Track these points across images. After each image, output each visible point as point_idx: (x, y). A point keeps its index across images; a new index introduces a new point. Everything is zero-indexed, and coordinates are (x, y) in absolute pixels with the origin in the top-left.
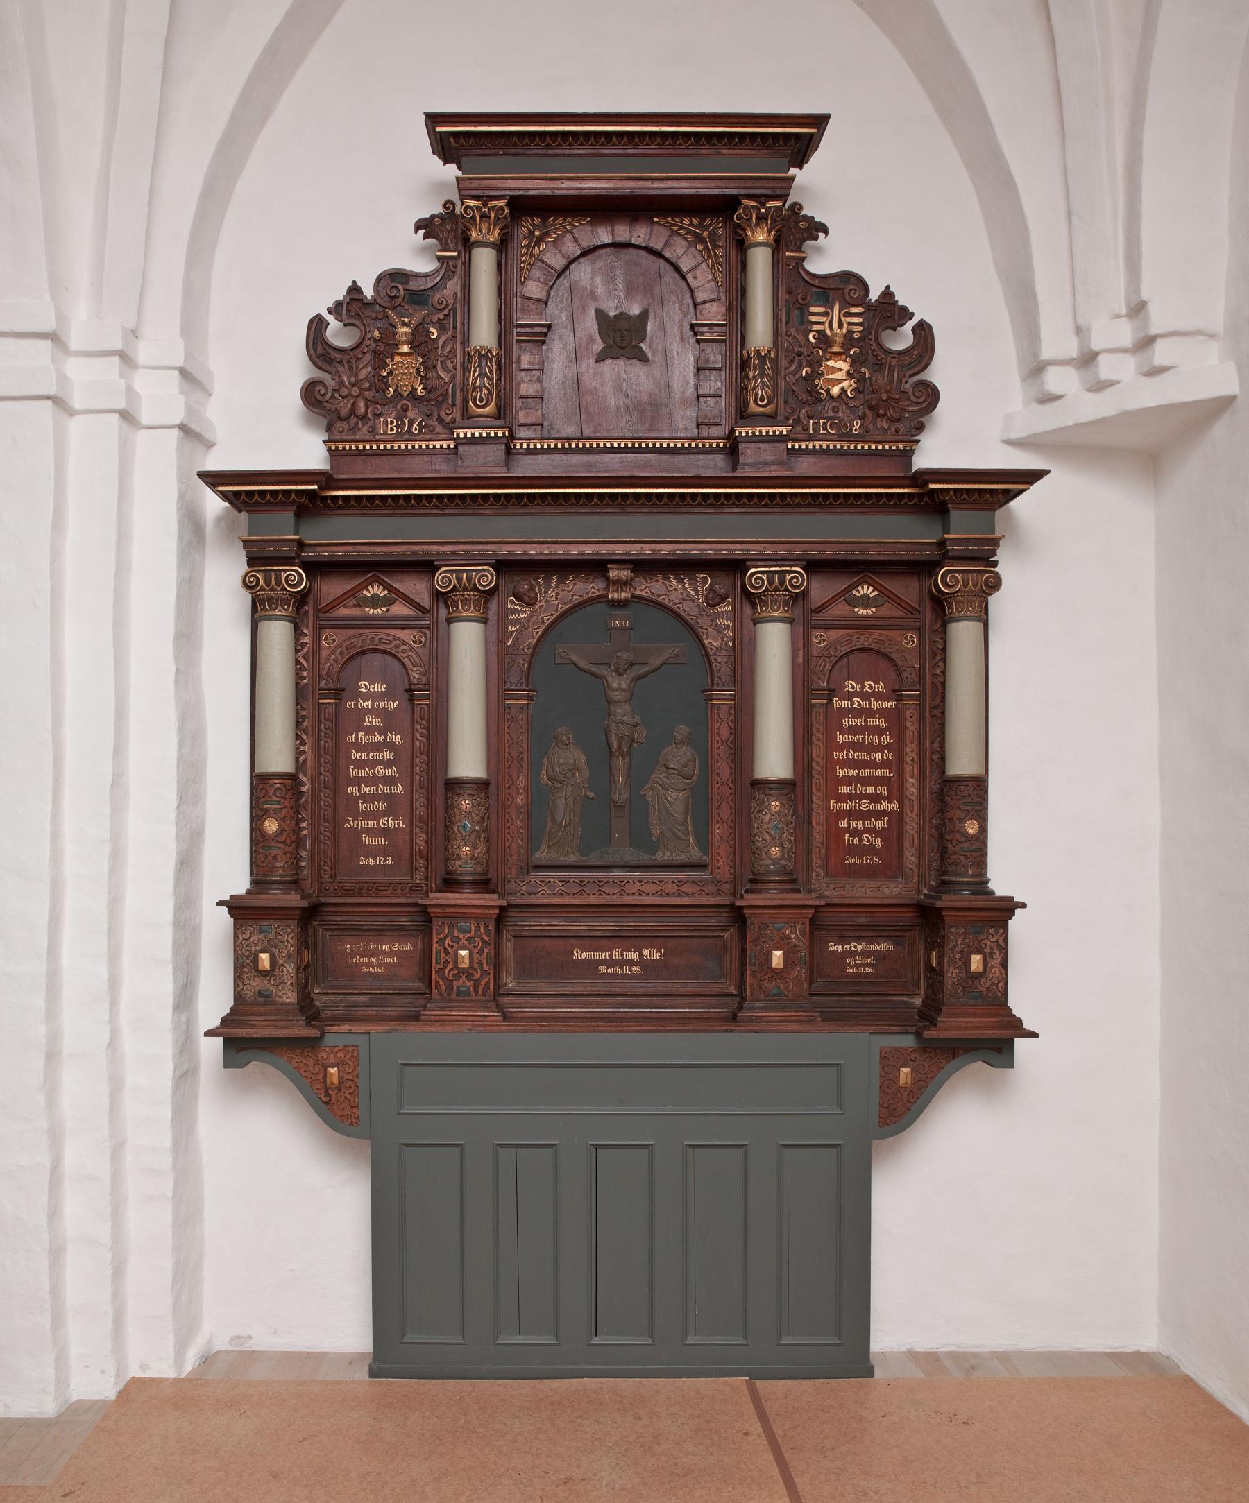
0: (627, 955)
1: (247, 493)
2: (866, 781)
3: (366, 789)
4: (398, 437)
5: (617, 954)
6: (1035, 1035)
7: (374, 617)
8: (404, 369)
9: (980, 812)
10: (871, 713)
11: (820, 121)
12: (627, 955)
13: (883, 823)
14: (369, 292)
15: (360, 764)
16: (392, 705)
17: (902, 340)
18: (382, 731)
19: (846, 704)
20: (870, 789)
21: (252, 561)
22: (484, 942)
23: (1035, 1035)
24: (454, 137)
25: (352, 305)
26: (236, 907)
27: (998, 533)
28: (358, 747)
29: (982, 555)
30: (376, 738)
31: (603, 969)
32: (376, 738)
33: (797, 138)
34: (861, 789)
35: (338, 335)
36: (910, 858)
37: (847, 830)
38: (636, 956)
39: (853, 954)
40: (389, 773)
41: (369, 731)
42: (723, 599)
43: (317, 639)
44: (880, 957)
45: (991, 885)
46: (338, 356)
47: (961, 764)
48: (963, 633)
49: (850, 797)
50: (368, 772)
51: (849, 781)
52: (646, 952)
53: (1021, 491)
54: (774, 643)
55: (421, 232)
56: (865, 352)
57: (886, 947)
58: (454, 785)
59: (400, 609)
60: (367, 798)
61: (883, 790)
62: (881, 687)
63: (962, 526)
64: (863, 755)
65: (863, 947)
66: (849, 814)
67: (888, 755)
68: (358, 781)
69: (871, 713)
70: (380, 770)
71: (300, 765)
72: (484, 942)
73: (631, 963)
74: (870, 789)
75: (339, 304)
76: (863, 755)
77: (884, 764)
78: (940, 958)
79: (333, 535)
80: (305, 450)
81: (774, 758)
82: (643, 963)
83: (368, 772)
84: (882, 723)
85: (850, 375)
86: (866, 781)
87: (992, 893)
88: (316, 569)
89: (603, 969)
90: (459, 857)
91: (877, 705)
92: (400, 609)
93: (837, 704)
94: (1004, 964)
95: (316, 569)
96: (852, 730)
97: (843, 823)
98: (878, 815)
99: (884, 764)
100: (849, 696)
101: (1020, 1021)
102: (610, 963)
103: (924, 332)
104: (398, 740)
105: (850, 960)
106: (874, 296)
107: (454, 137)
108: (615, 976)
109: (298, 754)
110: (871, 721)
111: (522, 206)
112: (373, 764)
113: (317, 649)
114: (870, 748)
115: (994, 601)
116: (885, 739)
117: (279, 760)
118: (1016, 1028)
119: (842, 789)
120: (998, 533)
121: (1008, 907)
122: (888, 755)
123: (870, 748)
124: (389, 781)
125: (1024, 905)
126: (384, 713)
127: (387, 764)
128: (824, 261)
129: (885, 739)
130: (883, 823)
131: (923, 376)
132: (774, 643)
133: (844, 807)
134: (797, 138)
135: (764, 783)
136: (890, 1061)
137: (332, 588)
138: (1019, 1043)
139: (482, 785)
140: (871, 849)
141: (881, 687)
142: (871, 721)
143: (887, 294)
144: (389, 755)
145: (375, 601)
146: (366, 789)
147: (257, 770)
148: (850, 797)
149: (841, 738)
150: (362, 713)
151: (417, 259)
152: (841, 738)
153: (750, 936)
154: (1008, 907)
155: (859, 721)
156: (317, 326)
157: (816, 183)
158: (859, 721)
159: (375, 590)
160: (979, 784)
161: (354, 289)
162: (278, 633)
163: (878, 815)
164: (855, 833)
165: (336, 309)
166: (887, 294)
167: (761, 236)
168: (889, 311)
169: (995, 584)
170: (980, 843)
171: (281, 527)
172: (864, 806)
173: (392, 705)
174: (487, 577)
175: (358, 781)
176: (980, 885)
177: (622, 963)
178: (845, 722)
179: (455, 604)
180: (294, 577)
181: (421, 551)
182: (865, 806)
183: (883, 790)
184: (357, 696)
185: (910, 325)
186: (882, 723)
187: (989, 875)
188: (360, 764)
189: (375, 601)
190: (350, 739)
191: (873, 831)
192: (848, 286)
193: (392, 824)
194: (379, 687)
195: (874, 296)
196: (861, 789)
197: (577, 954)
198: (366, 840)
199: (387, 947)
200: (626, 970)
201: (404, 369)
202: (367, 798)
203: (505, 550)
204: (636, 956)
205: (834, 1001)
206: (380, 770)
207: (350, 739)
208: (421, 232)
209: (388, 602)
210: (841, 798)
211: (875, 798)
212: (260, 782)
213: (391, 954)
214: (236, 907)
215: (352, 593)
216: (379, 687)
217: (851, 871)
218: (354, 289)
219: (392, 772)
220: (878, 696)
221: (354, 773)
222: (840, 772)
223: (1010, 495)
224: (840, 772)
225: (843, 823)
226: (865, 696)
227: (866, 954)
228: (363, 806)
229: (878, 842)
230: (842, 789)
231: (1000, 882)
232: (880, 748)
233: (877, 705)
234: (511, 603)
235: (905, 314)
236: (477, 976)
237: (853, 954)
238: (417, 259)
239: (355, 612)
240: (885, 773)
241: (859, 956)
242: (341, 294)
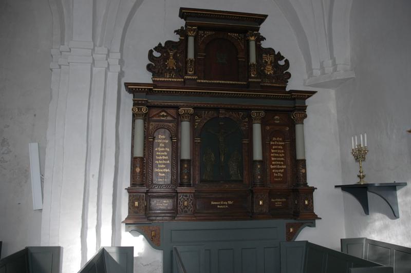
0: (224, 203)
1: (132, 88)
2: (278, 161)
3: (160, 162)
4: (169, 78)
5: (222, 203)
6: (321, 218)
7: (163, 120)
8: (171, 63)
9: (304, 167)
10: (279, 145)
11: (266, 16)
12: (224, 203)
13: (282, 171)
14: (163, 45)
15: (158, 156)
16: (167, 141)
17: (282, 63)
18: (165, 148)
19: (273, 143)
20: (280, 163)
21: (134, 105)
22: (191, 200)
23: (336, 187)
24: (185, 13)
25: (159, 48)
26: (128, 190)
27: (306, 104)
28: (158, 151)
29: (304, 108)
30: (163, 149)
31: (218, 206)
32: (163, 149)
33: (261, 19)
34: (277, 163)
35: (157, 54)
36: (289, 179)
37: (274, 172)
38: (226, 203)
39: (277, 202)
40: (166, 158)
41: (161, 147)
42: (245, 118)
43: (149, 125)
44: (282, 202)
45: (308, 185)
46: (155, 59)
47: (299, 157)
48: (298, 127)
49: (276, 165)
50: (160, 158)
51: (275, 161)
52: (229, 202)
53: (311, 96)
54: (257, 129)
55: (176, 33)
56: (276, 66)
57: (284, 200)
58: (182, 161)
59: (169, 118)
60: (160, 164)
61: (282, 163)
62: (281, 139)
63: (298, 103)
64: (277, 155)
65: (279, 200)
66: (275, 169)
67: (283, 155)
68: (158, 160)
69: (279, 145)
70: (164, 157)
71: (144, 155)
72: (191, 200)
73: (225, 205)
74: (280, 163)
75: (156, 47)
76: (277, 155)
77: (282, 157)
78: (298, 202)
79: (154, 100)
80: (146, 78)
81: (258, 155)
82: (228, 205)
83: (160, 158)
84: (281, 147)
85: (272, 70)
86: (278, 161)
87: (308, 186)
88: (150, 107)
89: (218, 206)
90: (184, 179)
91: (280, 143)
92: (169, 118)
93: (271, 143)
94: (313, 202)
95: (150, 107)
96: (275, 149)
97: (274, 171)
98: (281, 169)
99: (282, 157)
100: (274, 141)
101: (317, 215)
102: (220, 205)
103: (287, 62)
104: (168, 150)
105: (276, 203)
106: (276, 53)
107: (185, 13)
108: (221, 208)
109: (144, 153)
110: (279, 147)
111: (200, 28)
112: (162, 156)
113: (148, 128)
114: (279, 153)
115: (305, 120)
116: (282, 151)
117: (139, 153)
118: (316, 217)
119: (273, 163)
120: (306, 104)
121: (313, 189)
122: (283, 155)
123: (279, 153)
124: (165, 160)
125: (316, 188)
126: (165, 143)
127: (165, 156)
128: (265, 45)
129: (282, 151)
130: (282, 171)
131: (287, 71)
132: (257, 129)
133: (274, 167)
134: (261, 19)
135: (256, 161)
136: (288, 226)
137: (154, 111)
138: (317, 221)
139: (189, 161)
140: (280, 177)
141: (281, 139)
142: (279, 147)
143: (279, 53)
144: (166, 153)
145: (163, 116)
146: (160, 162)
147: (135, 156)
148: (276, 165)
149: (272, 151)
150: (159, 143)
151: (176, 38)
152: (272, 151)
153: (255, 196)
154: (313, 189)
155: (277, 147)
156: (151, 52)
157: (264, 29)
158: (277, 147)
159: (233, 107)
160: (304, 161)
161: (160, 44)
162: (140, 123)
163: (281, 169)
164: (276, 173)
165: (156, 49)
166: (279, 53)
167: (253, 38)
168: (279, 57)
169: (306, 116)
170: (305, 175)
171: (142, 98)
172: (278, 168)
173: (167, 141)
174: (191, 110)
175: (158, 160)
176: (306, 184)
177: (223, 205)
178: (273, 147)
179: (183, 117)
180: (144, 109)
181: (175, 104)
182: (278, 167)
183: (282, 163)
184: (158, 139)
185: (284, 60)
186: (281, 147)
187: (307, 182)
188: (158, 156)
189: (163, 116)
190: (156, 149)
191: (280, 172)
192: (270, 51)
193: (167, 171)
194: (164, 137)
195: (276, 53)
196: (277, 163)
197: (212, 203)
198: (160, 174)
199: (165, 201)
200: (224, 206)
201: (171, 63)
202: (160, 164)
203: (195, 105)
204: (226, 203)
205: (274, 213)
206: (164, 157)
207: (156, 149)
208: (176, 33)
209: (166, 116)
210: (273, 165)
211: (281, 165)
212: (134, 160)
213: (166, 203)
214: (128, 190)
215: (158, 114)
216: (164, 137)
217: (276, 182)
218: (160, 44)
219: (167, 158)
220: (280, 141)
221: (157, 158)
222: (273, 159)
223: (309, 97)
224: (273, 159)
225: (274, 171)
226: (277, 141)
227: (280, 202)
228: (159, 166)
229: (282, 175)
230: (273, 163)
231: (310, 184)
232: (281, 153)
233: (280, 143)
234: (196, 117)
235: (283, 58)
236: (189, 208)
237: (277, 202)
238: (176, 38)
239: (159, 118)
240: (283, 159)
241: (278, 202)
242: (157, 45)
